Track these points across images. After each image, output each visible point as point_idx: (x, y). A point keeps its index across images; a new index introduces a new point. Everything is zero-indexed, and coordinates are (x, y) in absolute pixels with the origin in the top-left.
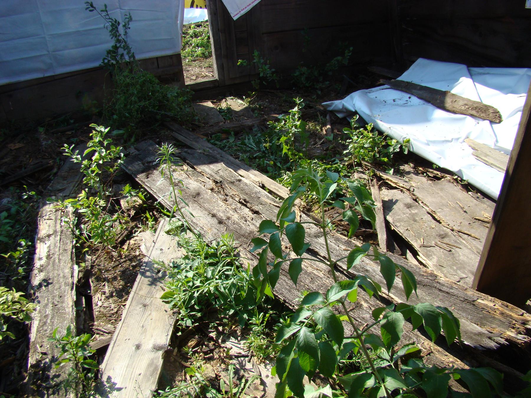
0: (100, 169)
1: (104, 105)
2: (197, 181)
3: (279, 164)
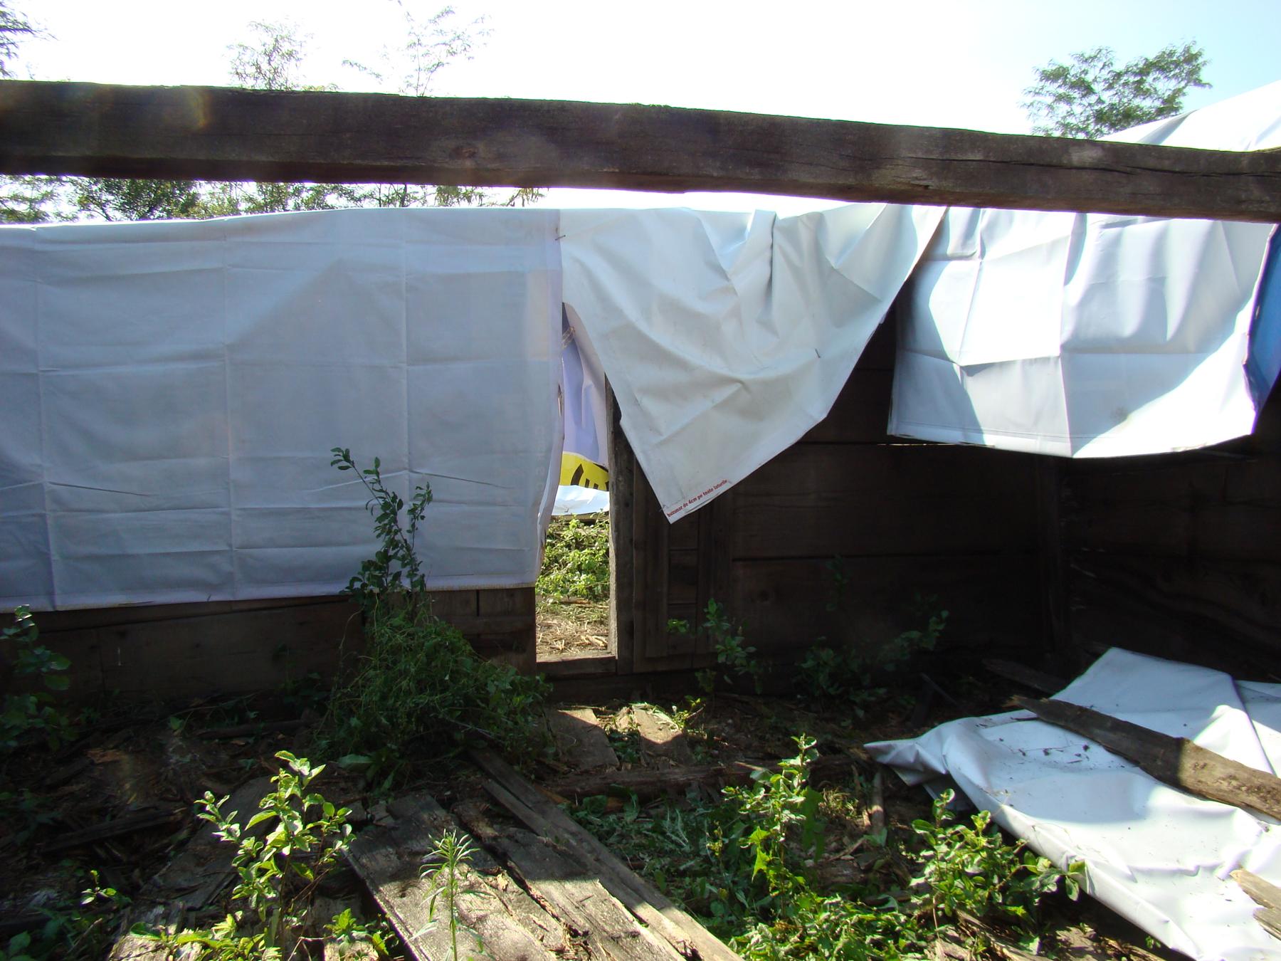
0: (281, 867)
1: (333, 690)
2: (524, 922)
3: (741, 897)
